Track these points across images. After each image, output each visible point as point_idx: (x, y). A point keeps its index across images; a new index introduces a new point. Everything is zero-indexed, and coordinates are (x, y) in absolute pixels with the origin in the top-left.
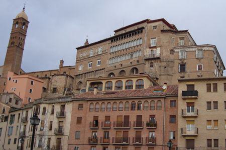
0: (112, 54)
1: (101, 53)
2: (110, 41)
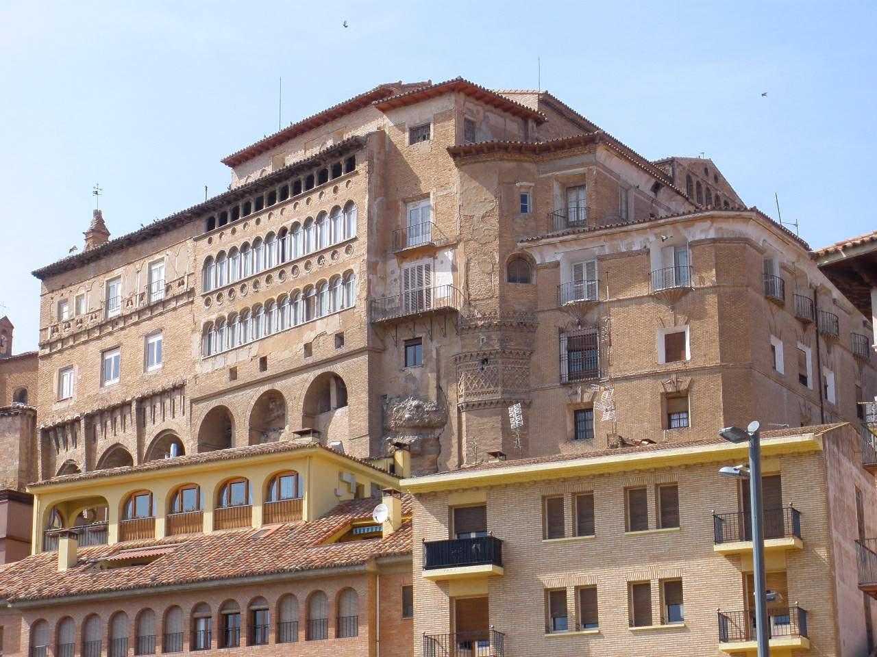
2: (202, 224)
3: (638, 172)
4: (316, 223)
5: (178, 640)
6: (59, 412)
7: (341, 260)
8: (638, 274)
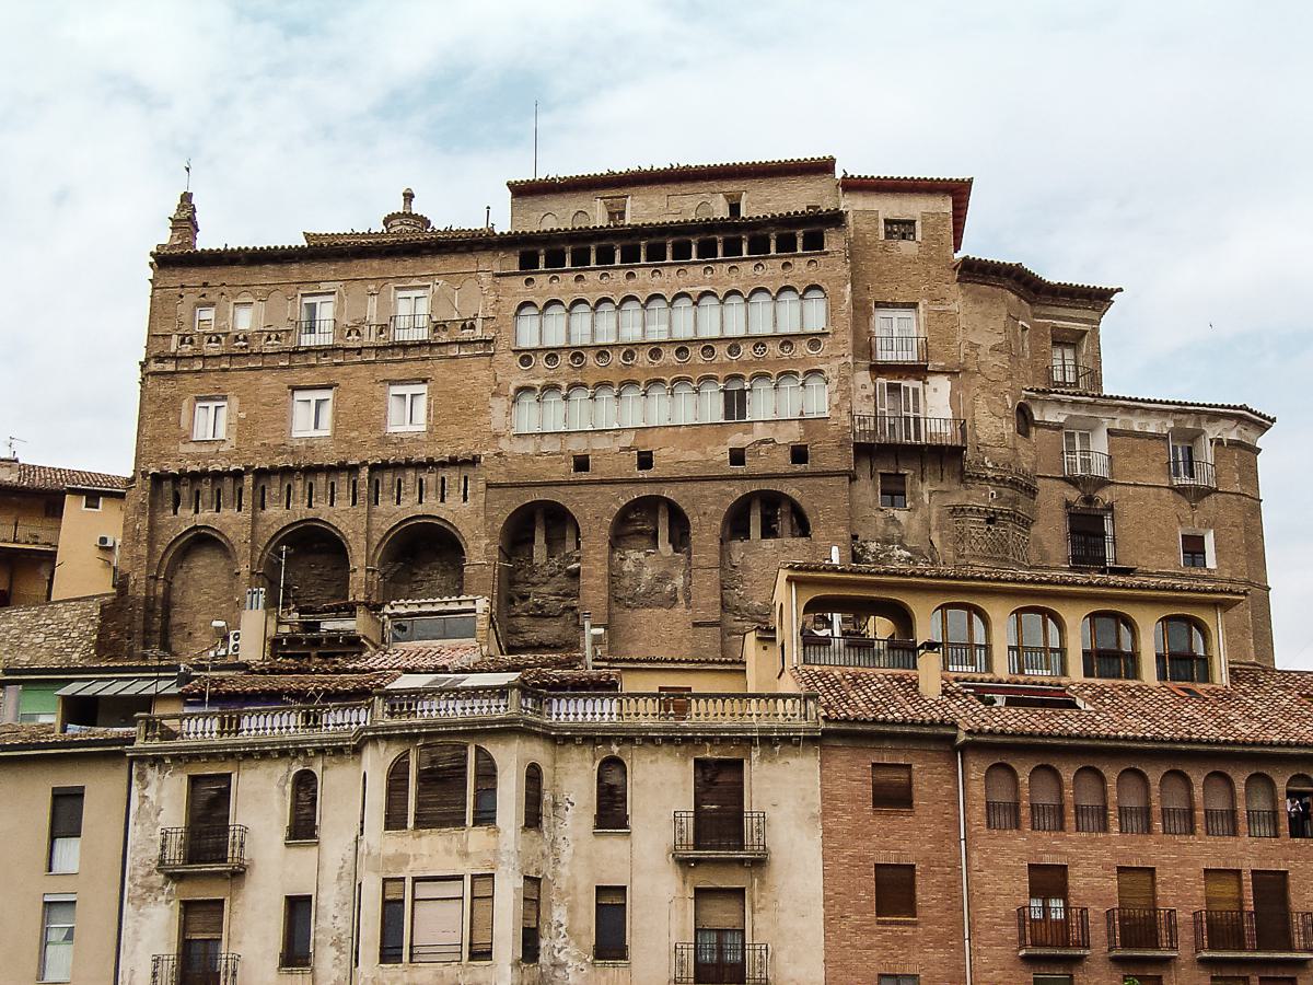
6: (195, 458)
8: (1154, 461)
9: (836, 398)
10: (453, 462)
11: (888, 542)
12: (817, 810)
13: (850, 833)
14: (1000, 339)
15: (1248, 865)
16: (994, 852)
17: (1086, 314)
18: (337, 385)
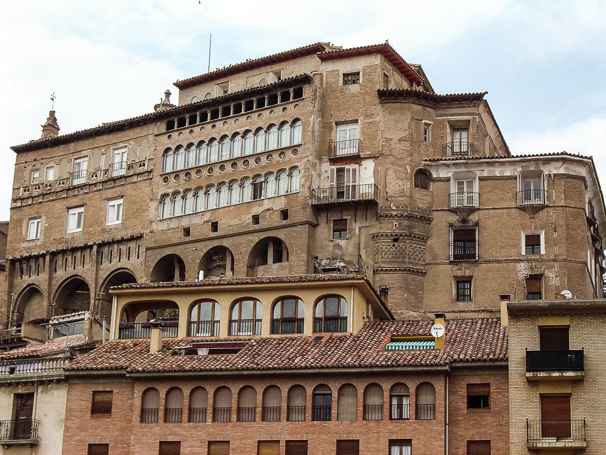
0: (172, 179)
1: (123, 172)
2: (162, 127)
3: (493, 126)
4: (208, 145)
5: (177, 414)
6: (26, 249)
7: (287, 159)
8: (508, 192)
9: (303, 180)
10: (132, 239)
11: (334, 259)
12: (63, 417)
13: (78, 428)
14: (405, 134)
15: (284, 437)
16: (143, 435)
17: (470, 110)
18: (86, 204)
